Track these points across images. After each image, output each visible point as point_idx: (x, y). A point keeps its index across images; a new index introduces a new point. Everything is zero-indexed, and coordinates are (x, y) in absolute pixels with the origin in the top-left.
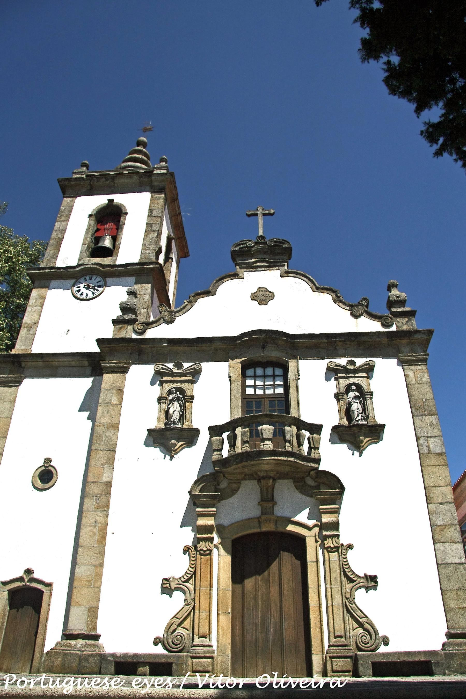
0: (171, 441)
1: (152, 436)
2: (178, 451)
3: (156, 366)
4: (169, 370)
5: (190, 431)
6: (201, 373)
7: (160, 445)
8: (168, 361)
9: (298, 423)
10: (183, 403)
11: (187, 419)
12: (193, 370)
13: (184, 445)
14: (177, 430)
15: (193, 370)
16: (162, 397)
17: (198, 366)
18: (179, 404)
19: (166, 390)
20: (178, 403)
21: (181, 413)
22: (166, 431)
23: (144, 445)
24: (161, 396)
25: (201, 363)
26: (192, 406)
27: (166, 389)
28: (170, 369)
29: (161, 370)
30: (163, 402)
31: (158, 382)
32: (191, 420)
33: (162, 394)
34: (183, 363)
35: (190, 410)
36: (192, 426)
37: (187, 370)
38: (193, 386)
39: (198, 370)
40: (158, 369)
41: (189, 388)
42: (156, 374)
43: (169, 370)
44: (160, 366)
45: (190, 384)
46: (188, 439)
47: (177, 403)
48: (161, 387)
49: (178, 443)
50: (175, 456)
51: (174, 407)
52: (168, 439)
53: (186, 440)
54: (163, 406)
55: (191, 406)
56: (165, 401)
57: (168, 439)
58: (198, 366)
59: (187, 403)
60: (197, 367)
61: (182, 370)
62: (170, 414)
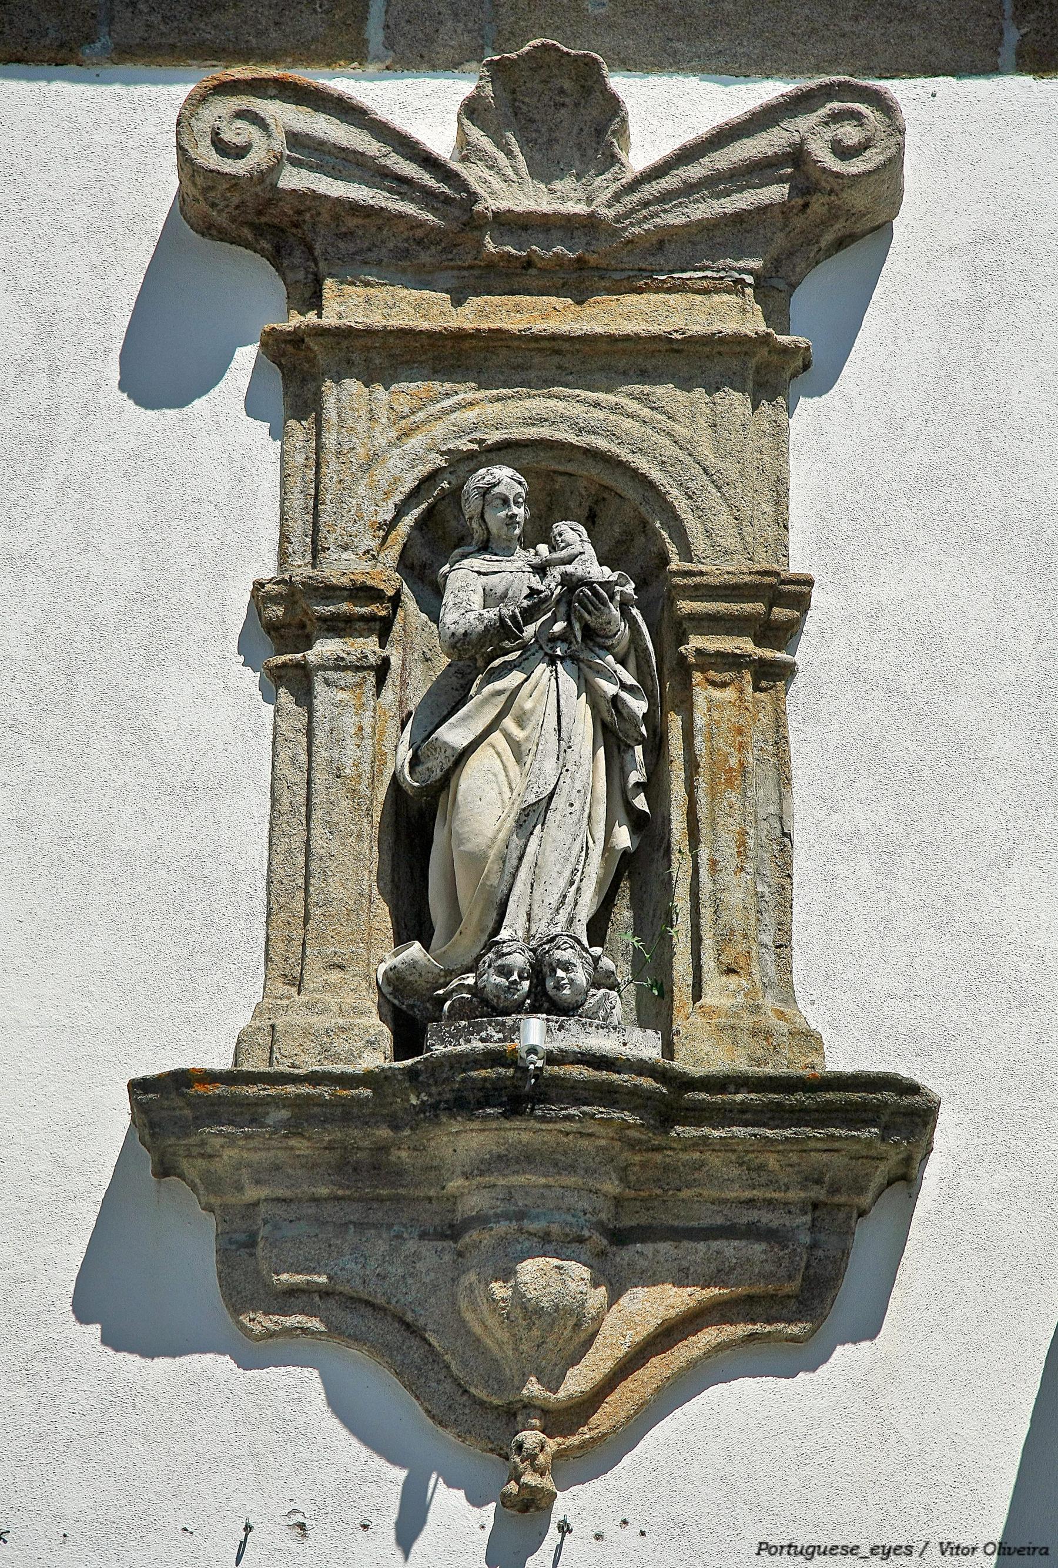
0: (507, 1274)
1: (212, 1183)
2: (602, 1420)
3: (224, 106)
4: (402, 185)
5: (776, 1115)
6: (882, 231)
7: (334, 1330)
8: (375, 33)
9: (611, 1387)
10: (644, 688)
11: (725, 939)
12: (775, 193)
13: (709, 1337)
14: (608, 1095)
15: (775, 193)
16: (329, 592)
17: (850, 133)
18: (594, 698)
19: (381, 475)
20: (586, 687)
21: (623, 838)
22: (433, 1111)
23: (83, 1312)
24: (301, 569)
25: (897, 89)
26: (781, 740)
27: (373, 459)
28: (429, 161)
29: (293, 179)
30: (339, 665)
31: (246, 356)
32: (782, 946)
33: (317, 550)
34: (618, 83)
35: (764, 793)
36: (809, 1039)
37: (689, 189)
38: (780, 433)
39: (856, 199)
40: (240, 152)
41: (730, 468)
42: (208, 230)
43: (402, 185)
44: (272, 109)
45: (735, 402)
46: (752, 1232)
47: (569, 684)
48: (299, 430)
49: (614, 1297)
50: (563, 1505)
51: (517, 749)
52: (452, 1231)
53: (729, 1248)
54: (349, 721)
55: (758, 740)
56: (369, 645)
57: (452, 1231)
58: (850, 133)
59: (702, 695)
60: (842, 152)
61: (605, 186)
62: (477, 860)
